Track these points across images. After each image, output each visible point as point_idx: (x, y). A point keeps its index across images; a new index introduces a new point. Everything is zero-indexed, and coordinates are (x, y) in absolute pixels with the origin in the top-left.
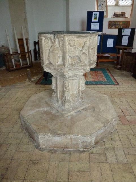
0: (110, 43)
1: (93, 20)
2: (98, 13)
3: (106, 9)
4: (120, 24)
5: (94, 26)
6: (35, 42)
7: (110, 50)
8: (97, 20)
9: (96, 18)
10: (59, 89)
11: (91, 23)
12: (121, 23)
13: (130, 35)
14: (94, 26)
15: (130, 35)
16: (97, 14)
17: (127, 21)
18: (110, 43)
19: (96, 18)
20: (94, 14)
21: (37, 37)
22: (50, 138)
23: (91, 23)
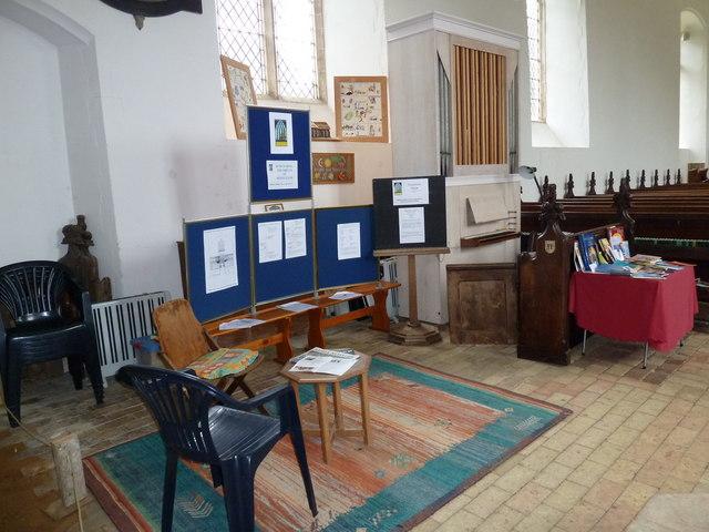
0: (349, 242)
1: (275, 149)
2: (288, 118)
3: (378, 100)
4: (323, 165)
5: (281, 174)
6: (535, 170)
7: (229, 302)
8: (289, 149)
9: (282, 139)
10: (403, 277)
11: (268, 162)
12: (328, 163)
13: (427, 202)
14: (281, 174)
15: (427, 202)
16: (285, 122)
17: (346, 155)
18: (349, 242)
19: (282, 139)
20: (276, 122)
21: (246, 209)
22: (139, 509)
23: (268, 162)
